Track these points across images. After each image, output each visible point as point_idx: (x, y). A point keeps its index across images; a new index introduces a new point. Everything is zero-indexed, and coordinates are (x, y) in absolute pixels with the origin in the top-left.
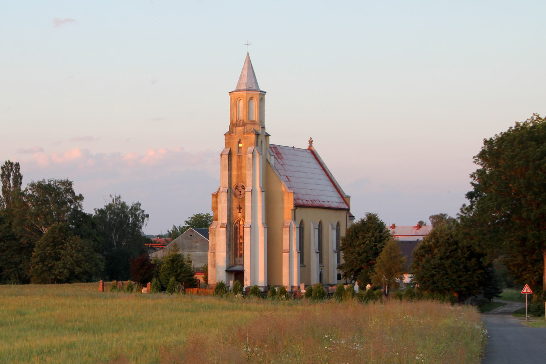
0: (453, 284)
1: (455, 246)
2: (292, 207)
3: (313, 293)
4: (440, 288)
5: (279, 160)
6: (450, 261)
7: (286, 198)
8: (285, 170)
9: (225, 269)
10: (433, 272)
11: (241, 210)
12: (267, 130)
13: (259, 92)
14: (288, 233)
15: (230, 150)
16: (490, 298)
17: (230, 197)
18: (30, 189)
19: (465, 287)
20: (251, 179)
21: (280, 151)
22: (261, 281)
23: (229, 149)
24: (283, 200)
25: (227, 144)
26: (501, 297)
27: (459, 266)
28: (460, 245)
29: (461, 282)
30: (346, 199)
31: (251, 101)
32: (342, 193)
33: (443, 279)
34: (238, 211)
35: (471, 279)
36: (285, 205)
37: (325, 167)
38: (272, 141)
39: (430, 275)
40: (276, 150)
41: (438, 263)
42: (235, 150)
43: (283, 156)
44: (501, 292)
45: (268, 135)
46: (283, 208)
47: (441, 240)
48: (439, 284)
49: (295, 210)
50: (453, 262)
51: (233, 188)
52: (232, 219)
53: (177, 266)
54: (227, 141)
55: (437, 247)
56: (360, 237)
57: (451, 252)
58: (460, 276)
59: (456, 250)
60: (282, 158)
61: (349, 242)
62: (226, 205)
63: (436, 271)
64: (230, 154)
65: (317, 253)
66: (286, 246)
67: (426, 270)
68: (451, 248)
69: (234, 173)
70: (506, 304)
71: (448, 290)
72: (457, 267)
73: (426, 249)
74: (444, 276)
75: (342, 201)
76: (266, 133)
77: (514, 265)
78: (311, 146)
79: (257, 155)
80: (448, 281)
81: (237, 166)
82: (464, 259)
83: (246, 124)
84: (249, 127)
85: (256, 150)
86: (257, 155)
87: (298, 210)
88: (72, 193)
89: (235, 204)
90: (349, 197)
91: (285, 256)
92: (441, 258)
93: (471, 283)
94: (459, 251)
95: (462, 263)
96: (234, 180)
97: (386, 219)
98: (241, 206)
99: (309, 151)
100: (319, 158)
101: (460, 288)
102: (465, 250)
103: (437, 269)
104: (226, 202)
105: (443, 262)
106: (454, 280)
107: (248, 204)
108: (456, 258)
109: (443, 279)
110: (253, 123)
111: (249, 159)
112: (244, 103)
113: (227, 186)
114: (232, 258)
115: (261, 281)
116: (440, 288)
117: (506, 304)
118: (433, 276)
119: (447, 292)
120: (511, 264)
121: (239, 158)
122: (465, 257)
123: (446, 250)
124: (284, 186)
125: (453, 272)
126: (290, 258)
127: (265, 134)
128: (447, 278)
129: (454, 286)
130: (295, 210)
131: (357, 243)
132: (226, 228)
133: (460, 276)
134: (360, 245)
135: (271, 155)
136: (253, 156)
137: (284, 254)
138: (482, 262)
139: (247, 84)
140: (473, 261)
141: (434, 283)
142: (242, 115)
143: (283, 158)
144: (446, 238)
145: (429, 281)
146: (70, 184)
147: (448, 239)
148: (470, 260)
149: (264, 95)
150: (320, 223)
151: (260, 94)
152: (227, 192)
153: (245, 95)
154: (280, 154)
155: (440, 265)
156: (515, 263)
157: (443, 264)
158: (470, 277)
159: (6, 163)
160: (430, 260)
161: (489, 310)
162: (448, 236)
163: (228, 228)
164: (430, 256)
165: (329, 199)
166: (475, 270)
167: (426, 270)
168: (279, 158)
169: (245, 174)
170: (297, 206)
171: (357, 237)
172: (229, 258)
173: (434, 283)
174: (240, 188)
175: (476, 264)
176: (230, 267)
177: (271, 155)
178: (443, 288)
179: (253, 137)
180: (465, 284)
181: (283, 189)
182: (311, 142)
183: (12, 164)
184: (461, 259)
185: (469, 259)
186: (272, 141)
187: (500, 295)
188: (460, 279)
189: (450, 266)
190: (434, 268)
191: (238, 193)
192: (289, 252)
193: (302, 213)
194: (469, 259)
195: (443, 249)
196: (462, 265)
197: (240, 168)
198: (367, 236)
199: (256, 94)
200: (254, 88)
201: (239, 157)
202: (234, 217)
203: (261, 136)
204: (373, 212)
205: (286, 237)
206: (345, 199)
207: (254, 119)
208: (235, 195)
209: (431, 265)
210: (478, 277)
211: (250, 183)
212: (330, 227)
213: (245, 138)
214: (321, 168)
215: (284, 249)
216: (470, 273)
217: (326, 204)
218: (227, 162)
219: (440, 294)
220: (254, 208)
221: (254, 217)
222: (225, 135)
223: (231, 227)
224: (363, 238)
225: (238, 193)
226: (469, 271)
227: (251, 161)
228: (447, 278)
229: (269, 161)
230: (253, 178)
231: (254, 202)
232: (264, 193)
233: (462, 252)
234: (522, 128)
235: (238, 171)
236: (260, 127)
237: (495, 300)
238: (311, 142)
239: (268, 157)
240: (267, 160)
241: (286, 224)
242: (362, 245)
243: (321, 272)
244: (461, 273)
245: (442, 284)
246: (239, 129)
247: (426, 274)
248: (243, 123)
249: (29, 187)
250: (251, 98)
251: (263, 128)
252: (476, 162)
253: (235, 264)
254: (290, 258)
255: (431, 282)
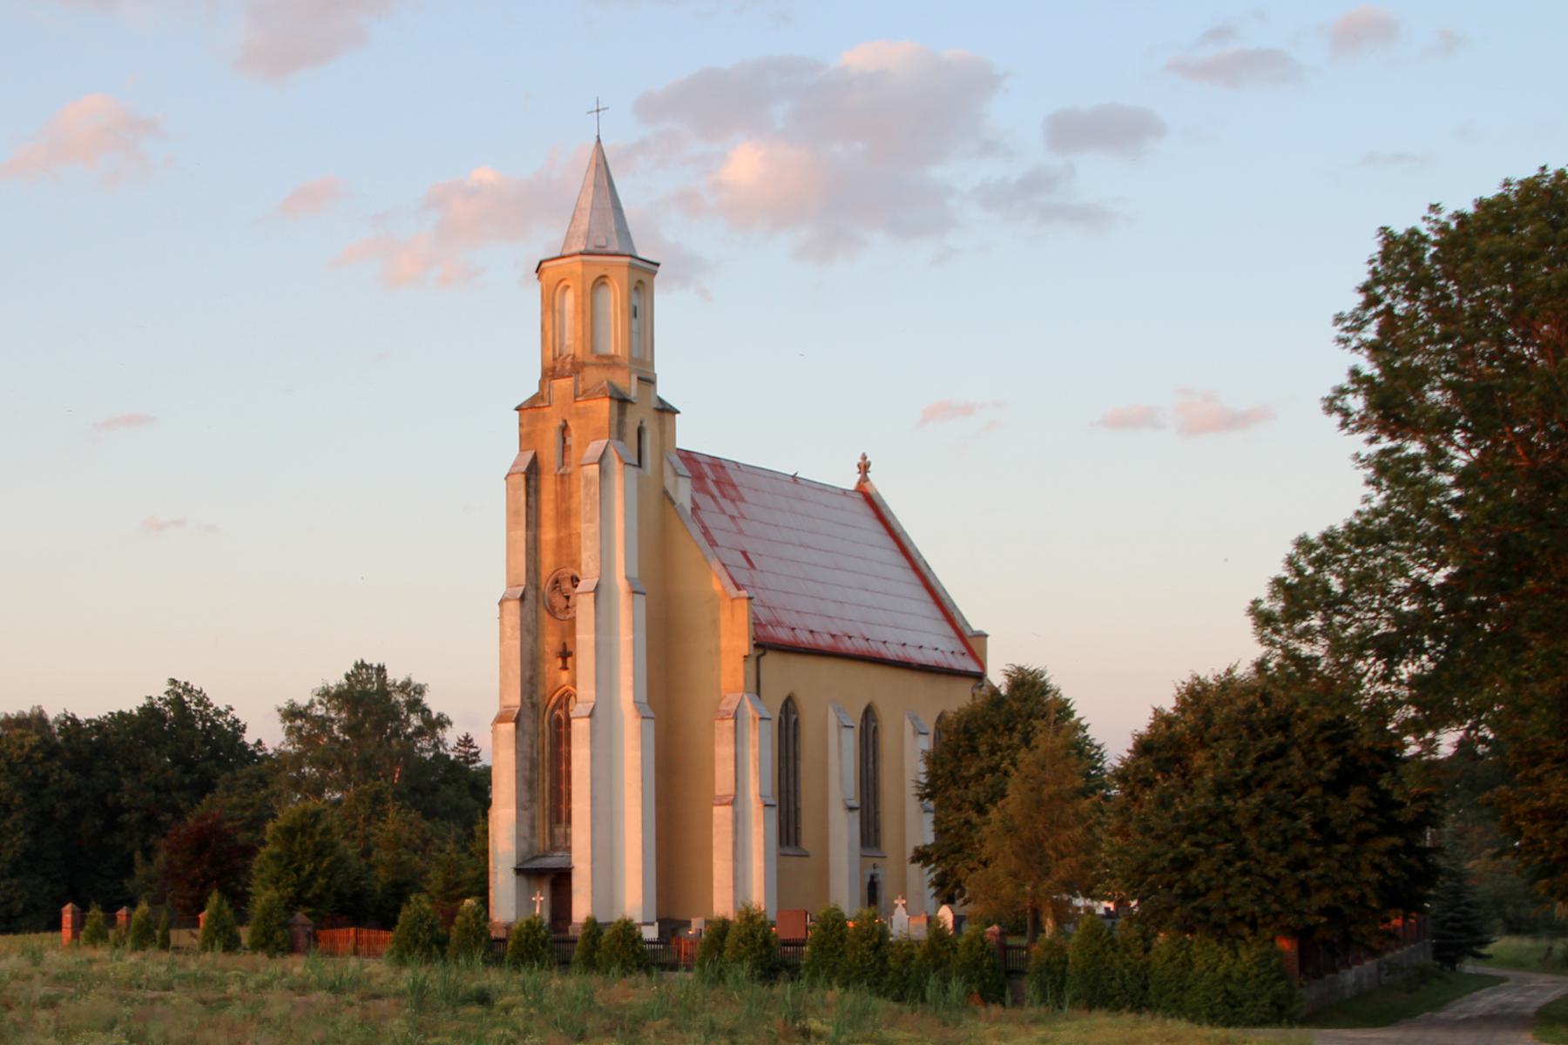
0: (1269, 899)
1: (1278, 737)
2: (744, 645)
3: (731, 939)
4: (1215, 916)
5: (725, 503)
6: (1256, 799)
7: (724, 617)
8: (740, 532)
9: (513, 863)
10: (1184, 845)
11: (569, 660)
12: (665, 390)
13: (627, 260)
14: (730, 736)
15: (535, 457)
16: (1452, 962)
17: (537, 620)
18: (321, 703)
19: (1321, 912)
20: (596, 551)
21: (735, 477)
22: (633, 899)
23: (529, 455)
24: (715, 623)
25: (526, 439)
26: (1489, 956)
27: (1295, 818)
28: (1300, 729)
29: (1304, 888)
30: (974, 643)
31: (602, 290)
32: (960, 623)
33: (1228, 877)
34: (560, 662)
35: (1348, 875)
36: (724, 643)
37: (906, 543)
38: (690, 435)
39: (1173, 860)
40: (711, 475)
41: (1204, 809)
42: (550, 455)
43: (744, 492)
44: (1488, 942)
45: (666, 411)
46: (718, 651)
47: (1220, 715)
48: (1213, 900)
49: (758, 659)
50: (1268, 802)
51: (546, 586)
52: (541, 691)
53: (305, 852)
54: (525, 430)
55: (1203, 745)
56: (983, 748)
57: (1261, 760)
58: (1300, 864)
59: (1281, 751)
60: (737, 499)
61: (948, 767)
62: (518, 643)
63: (1197, 844)
64: (532, 473)
65: (851, 809)
66: (723, 781)
67: (1158, 838)
68: (1259, 745)
69: (548, 534)
70: (1504, 980)
71: (1253, 925)
72: (1284, 821)
73: (1163, 755)
74: (1230, 863)
75: (961, 648)
76: (661, 401)
77: (1533, 815)
78: (864, 479)
79: (616, 466)
80: (1247, 885)
81: (557, 508)
82: (1317, 791)
83: (584, 365)
84: (593, 376)
85: (611, 450)
86: (616, 466)
87: (771, 661)
88: (425, 711)
89: (551, 643)
90: (982, 636)
91: (721, 816)
92: (1220, 789)
93: (1352, 893)
94: (1295, 755)
95: (1308, 806)
96: (548, 560)
97: (1064, 681)
98: (569, 649)
99: (859, 496)
100: (889, 518)
101: (1301, 914)
102: (1322, 752)
103: (1202, 837)
104: (518, 633)
105: (1227, 801)
106: (1275, 881)
107: (585, 638)
108: (1283, 786)
109: (1228, 877)
110: (609, 362)
111: (588, 482)
112: (576, 297)
113: (522, 579)
114: (543, 826)
115: (633, 899)
116: (1215, 916)
117: (1504, 980)
118: (1183, 864)
119: (1246, 931)
120: (1523, 808)
121: (562, 482)
122: (1321, 783)
123: (1241, 752)
124: (719, 578)
125: (1272, 848)
126: (738, 822)
127: (656, 404)
128: (1245, 872)
129: (1276, 907)
130: (758, 659)
131: (973, 771)
132: (517, 721)
133: (1300, 864)
134: (980, 775)
135: (677, 475)
136: (603, 472)
137: (716, 810)
138: (1388, 792)
139: (588, 235)
140: (1357, 796)
141: (1189, 894)
142: (571, 341)
143: (742, 499)
144: (1241, 704)
145: (1170, 886)
146: (420, 690)
147: (1251, 709)
148: (1344, 796)
149: (654, 273)
150: (869, 713)
151: (631, 266)
152: (522, 598)
153: (579, 269)
154: (734, 486)
155: (1214, 818)
156: (1540, 804)
157: (1227, 811)
158: (1343, 867)
159: (356, 666)
160: (1173, 797)
161: (1438, 1006)
162: (1251, 698)
163: (527, 723)
164: (1175, 779)
165: (910, 638)
166: (1363, 837)
167: (1158, 838)
168: (724, 496)
169: (579, 535)
170: (764, 645)
171: (974, 750)
172: (532, 828)
173: (1189, 894)
174: (567, 585)
175: (1367, 810)
176: (534, 858)
177: (677, 475)
178: (1228, 916)
179: (603, 408)
180: (1326, 897)
181: (716, 587)
182: (864, 467)
183: (368, 667)
184: (1303, 790)
185: (1338, 786)
186: (690, 435)
187: (1484, 951)
188: (1302, 875)
189: (1257, 821)
190: (1192, 830)
191: (559, 602)
192: (733, 803)
193: (783, 674)
194: (1338, 786)
195: (1227, 751)
196: (1307, 815)
197: (565, 516)
198: (1003, 742)
199: (619, 265)
200: (614, 248)
201: (563, 479)
202: (549, 684)
203: (638, 414)
204: (1031, 663)
205: (724, 751)
206: (972, 643)
207: (612, 351)
208: (552, 611)
209: (1176, 817)
210: (1375, 867)
211: (591, 565)
212: (909, 729)
213: (579, 415)
214: (895, 546)
215: (718, 793)
216: (1344, 848)
217: (892, 652)
218: (523, 499)
219: (1220, 942)
220: (604, 652)
221: (605, 680)
222: (518, 409)
223: (537, 719)
224: (992, 753)
225: (559, 602)
226: (1340, 840)
227: (595, 489)
228: (1245, 872)
229: (672, 493)
230: (607, 545)
231: (604, 627)
232: (641, 600)
233: (1309, 763)
234: (1547, 191)
235: (558, 527)
236: (634, 378)
237: (1469, 966)
238: (864, 467)
239: (669, 481)
240: (665, 493)
241: (723, 707)
242: (988, 775)
243: (872, 877)
244: (1304, 850)
245: (1226, 897)
246: (563, 385)
247: (1155, 856)
248: (573, 364)
249: (316, 699)
250: (601, 281)
251: (648, 381)
252: (1345, 341)
253: (554, 848)
254: (738, 822)
255: (1176, 890)
